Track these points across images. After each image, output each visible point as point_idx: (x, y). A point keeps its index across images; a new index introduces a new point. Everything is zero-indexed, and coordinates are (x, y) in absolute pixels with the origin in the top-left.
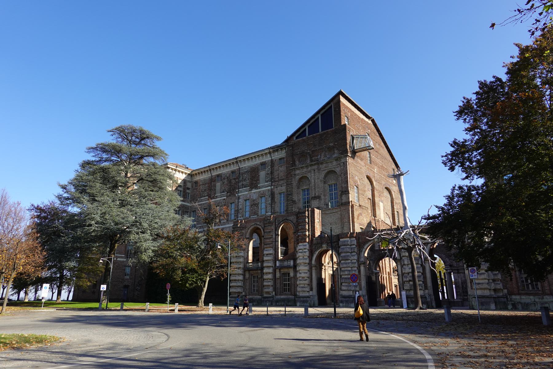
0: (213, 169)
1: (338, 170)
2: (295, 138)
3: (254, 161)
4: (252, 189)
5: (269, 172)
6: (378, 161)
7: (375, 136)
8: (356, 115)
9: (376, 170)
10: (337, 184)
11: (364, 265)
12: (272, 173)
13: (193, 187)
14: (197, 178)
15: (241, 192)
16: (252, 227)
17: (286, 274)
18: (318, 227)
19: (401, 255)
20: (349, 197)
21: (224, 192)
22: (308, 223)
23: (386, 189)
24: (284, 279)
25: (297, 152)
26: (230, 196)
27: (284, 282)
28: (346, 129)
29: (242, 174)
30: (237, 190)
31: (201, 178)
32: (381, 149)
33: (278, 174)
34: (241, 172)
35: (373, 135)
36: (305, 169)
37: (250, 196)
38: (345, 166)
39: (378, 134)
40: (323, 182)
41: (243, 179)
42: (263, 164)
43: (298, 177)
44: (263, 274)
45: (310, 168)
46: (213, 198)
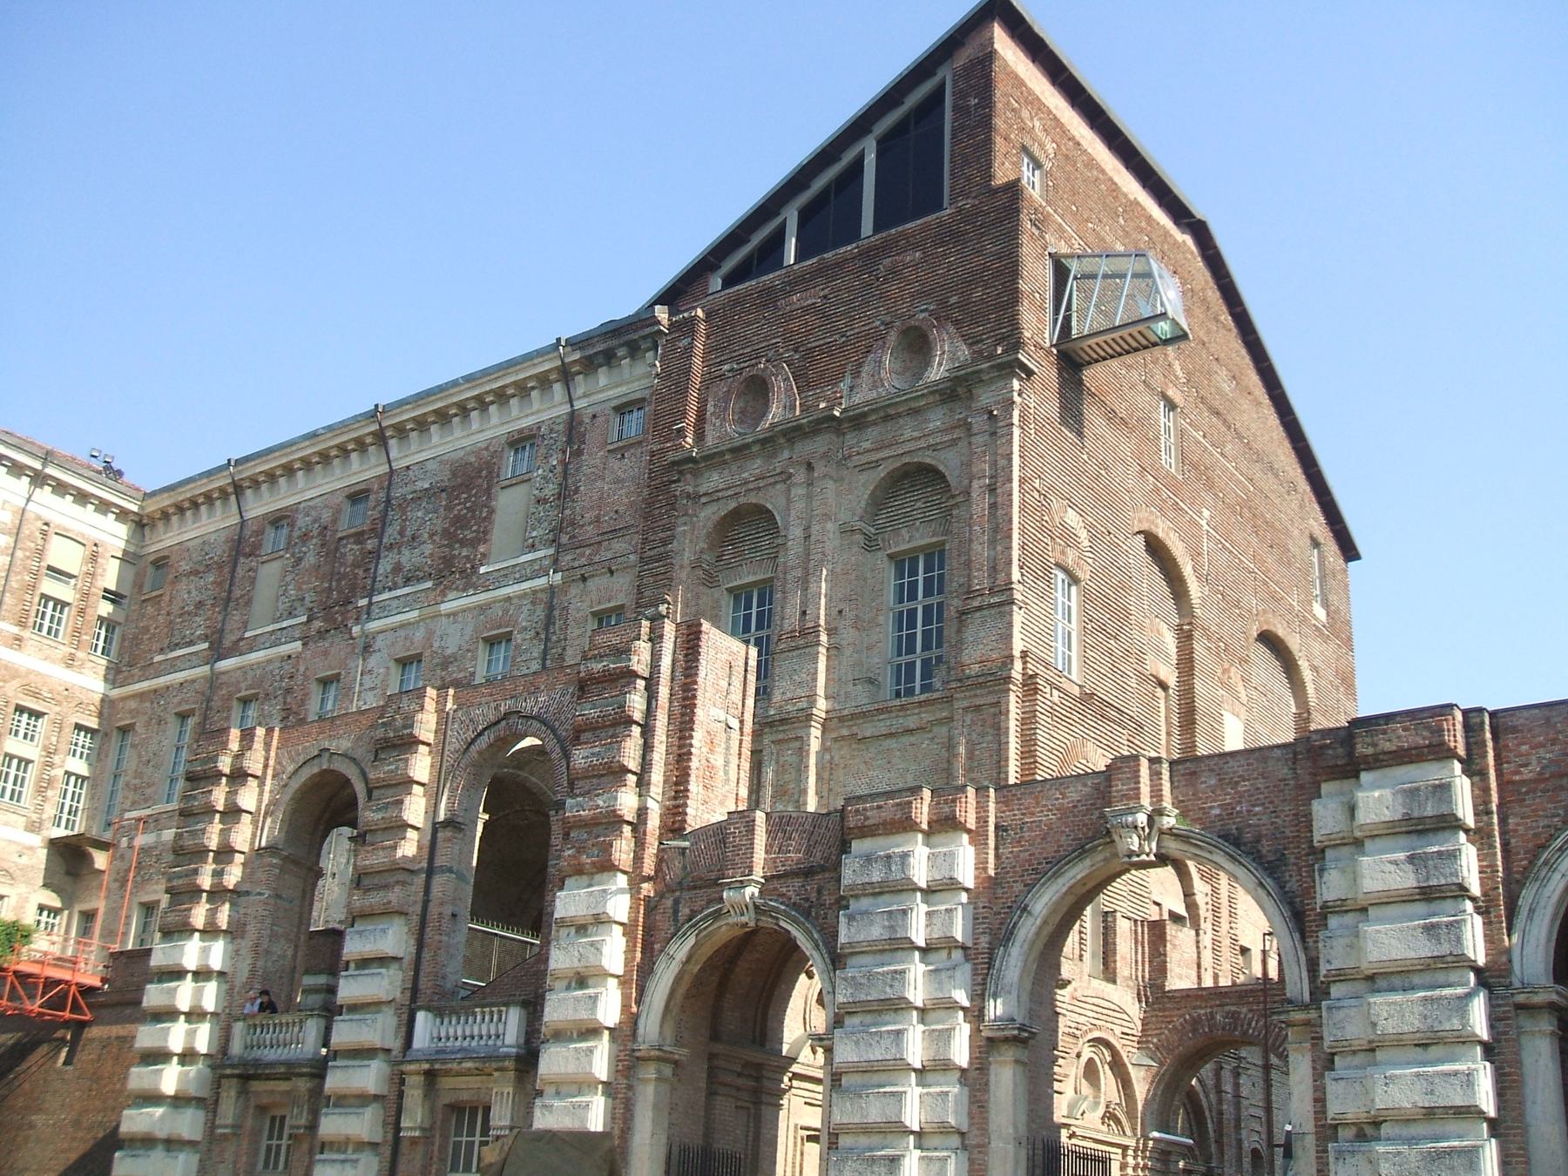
0: (255, 483)
1: (948, 461)
2: (716, 282)
3: (475, 426)
5: (550, 490)
8: (1091, 163)
9: (1206, 513)
10: (942, 552)
11: (1023, 1054)
12: (565, 494)
13: (141, 587)
14: (166, 539)
15: (386, 611)
17: (476, 1109)
18: (718, 761)
19: (1323, 969)
20: (1010, 625)
21: (291, 615)
22: (647, 730)
25: (721, 363)
26: (322, 634)
28: (1018, 211)
29: (404, 504)
30: (363, 602)
31: (186, 537)
32: (1245, 404)
34: (397, 493)
37: (430, 634)
39: (1226, 318)
40: (859, 537)
41: (401, 533)
42: (520, 441)
43: (709, 515)
44: (318, 1101)
45: (786, 454)
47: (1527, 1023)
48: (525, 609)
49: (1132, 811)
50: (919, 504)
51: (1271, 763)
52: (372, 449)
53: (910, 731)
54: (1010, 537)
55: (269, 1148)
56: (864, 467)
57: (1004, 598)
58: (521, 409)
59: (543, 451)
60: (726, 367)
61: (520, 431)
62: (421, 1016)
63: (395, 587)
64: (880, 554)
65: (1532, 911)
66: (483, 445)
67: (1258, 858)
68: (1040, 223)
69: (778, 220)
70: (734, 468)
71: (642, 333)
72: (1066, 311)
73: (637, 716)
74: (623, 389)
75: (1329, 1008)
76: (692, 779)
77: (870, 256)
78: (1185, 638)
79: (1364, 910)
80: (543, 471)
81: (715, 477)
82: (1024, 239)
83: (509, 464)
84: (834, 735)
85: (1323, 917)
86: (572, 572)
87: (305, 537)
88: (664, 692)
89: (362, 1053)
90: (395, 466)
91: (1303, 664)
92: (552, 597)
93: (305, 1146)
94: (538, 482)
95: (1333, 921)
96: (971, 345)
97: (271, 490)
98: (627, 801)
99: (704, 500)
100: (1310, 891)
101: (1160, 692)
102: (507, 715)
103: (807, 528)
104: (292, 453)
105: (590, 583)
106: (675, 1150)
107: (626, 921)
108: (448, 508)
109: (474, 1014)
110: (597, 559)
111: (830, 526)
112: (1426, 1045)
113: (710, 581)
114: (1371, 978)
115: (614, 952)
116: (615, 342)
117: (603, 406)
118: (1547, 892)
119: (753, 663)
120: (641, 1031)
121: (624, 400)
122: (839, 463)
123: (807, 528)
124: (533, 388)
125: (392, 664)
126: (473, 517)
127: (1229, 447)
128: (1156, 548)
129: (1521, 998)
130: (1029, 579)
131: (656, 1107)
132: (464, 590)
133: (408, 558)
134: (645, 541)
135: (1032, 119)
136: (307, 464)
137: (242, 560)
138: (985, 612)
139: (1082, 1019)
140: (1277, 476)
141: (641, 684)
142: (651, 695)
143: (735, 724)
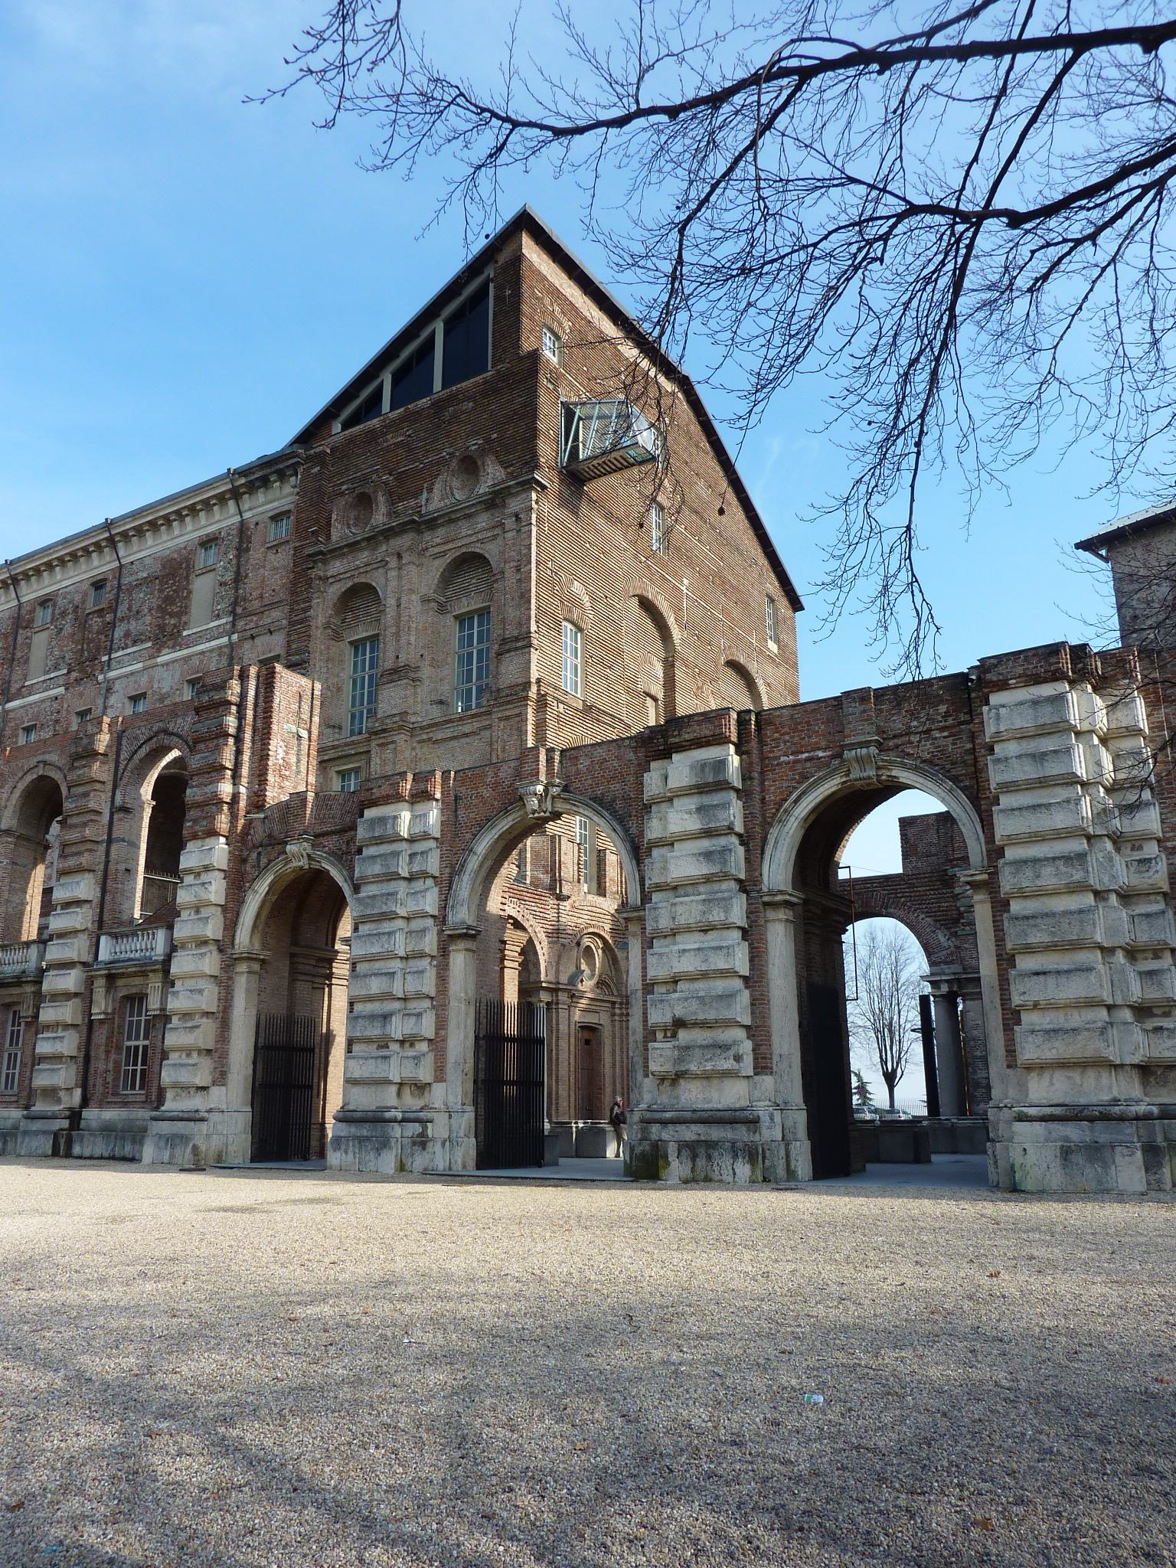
0: (26, 576)
1: (491, 551)
3: (177, 532)
4: (159, 651)
5: (229, 576)
6: (702, 550)
7: (694, 450)
9: (686, 581)
11: (470, 944)
12: (238, 579)
15: (121, 663)
16: (29, 778)
19: (647, 883)
21: (56, 668)
22: (239, 740)
23: (729, 671)
24: (131, 1023)
25: (342, 484)
26: (78, 681)
27: (129, 1039)
28: (537, 372)
30: (105, 658)
33: (263, 581)
34: (125, 581)
35: (684, 441)
36: (366, 553)
37: (151, 681)
38: (524, 529)
41: (130, 609)
42: (208, 542)
43: (335, 591)
44: (39, 997)
45: (384, 547)
46: (19, 695)
47: (771, 914)
48: (214, 660)
49: (532, 784)
50: (474, 581)
51: (623, 749)
52: (106, 550)
53: (466, 735)
54: (529, 602)
55: (12, 1032)
56: (437, 556)
57: (525, 643)
58: (207, 519)
59: (223, 548)
60: (344, 487)
61: (207, 535)
62: (103, 939)
63: (127, 647)
64: (448, 615)
65: (776, 842)
66: (183, 546)
67: (614, 813)
68: (555, 379)
69: (376, 383)
70: (350, 557)
71: (286, 464)
72: (573, 442)
73: (232, 731)
74: (276, 504)
75: (650, 910)
76: (270, 771)
77: (439, 406)
78: (669, 666)
79: (672, 844)
80: (220, 561)
81: (338, 564)
82: (541, 392)
83: (201, 559)
84: (418, 739)
85: (650, 849)
86: (245, 633)
87: (63, 614)
88: (250, 713)
89: (66, 965)
90: (123, 561)
91: (760, 682)
92: (232, 651)
93: (33, 1029)
94: (220, 571)
95: (655, 852)
96: (506, 468)
97: (38, 581)
98: (226, 789)
99: (331, 580)
100: (642, 833)
101: (649, 702)
102: (157, 734)
103: (399, 599)
104: (50, 554)
105: (257, 640)
106: (263, 1017)
107: (226, 868)
108: (161, 591)
109: (138, 935)
110: (261, 623)
111: (414, 597)
112: (707, 931)
113: (337, 637)
114: (675, 888)
115: (216, 889)
116: (268, 471)
117: (263, 516)
118: (786, 829)
119: (317, 693)
120: (237, 941)
121: (277, 511)
122: (419, 554)
123: (399, 599)
124: (214, 504)
125: (126, 700)
126: (178, 596)
127: (705, 535)
128: (647, 605)
129: (766, 899)
130: (543, 629)
131: (248, 990)
132: (173, 647)
133: (134, 626)
134: (292, 611)
135: (552, 305)
136: (62, 561)
137: (21, 631)
138: (513, 653)
139: (580, 921)
140: (742, 555)
141: (234, 709)
142: (241, 717)
143: (304, 734)
